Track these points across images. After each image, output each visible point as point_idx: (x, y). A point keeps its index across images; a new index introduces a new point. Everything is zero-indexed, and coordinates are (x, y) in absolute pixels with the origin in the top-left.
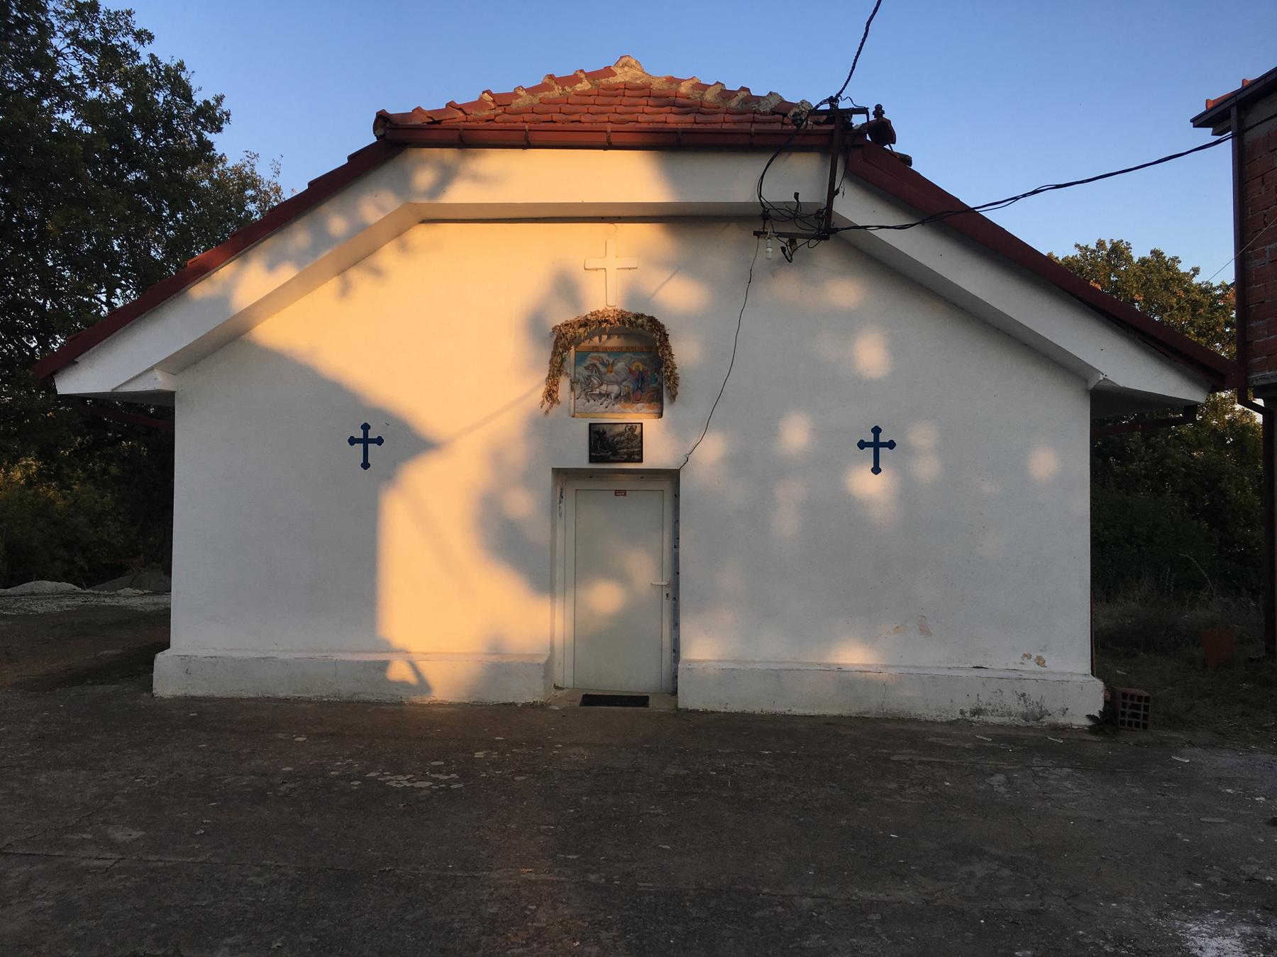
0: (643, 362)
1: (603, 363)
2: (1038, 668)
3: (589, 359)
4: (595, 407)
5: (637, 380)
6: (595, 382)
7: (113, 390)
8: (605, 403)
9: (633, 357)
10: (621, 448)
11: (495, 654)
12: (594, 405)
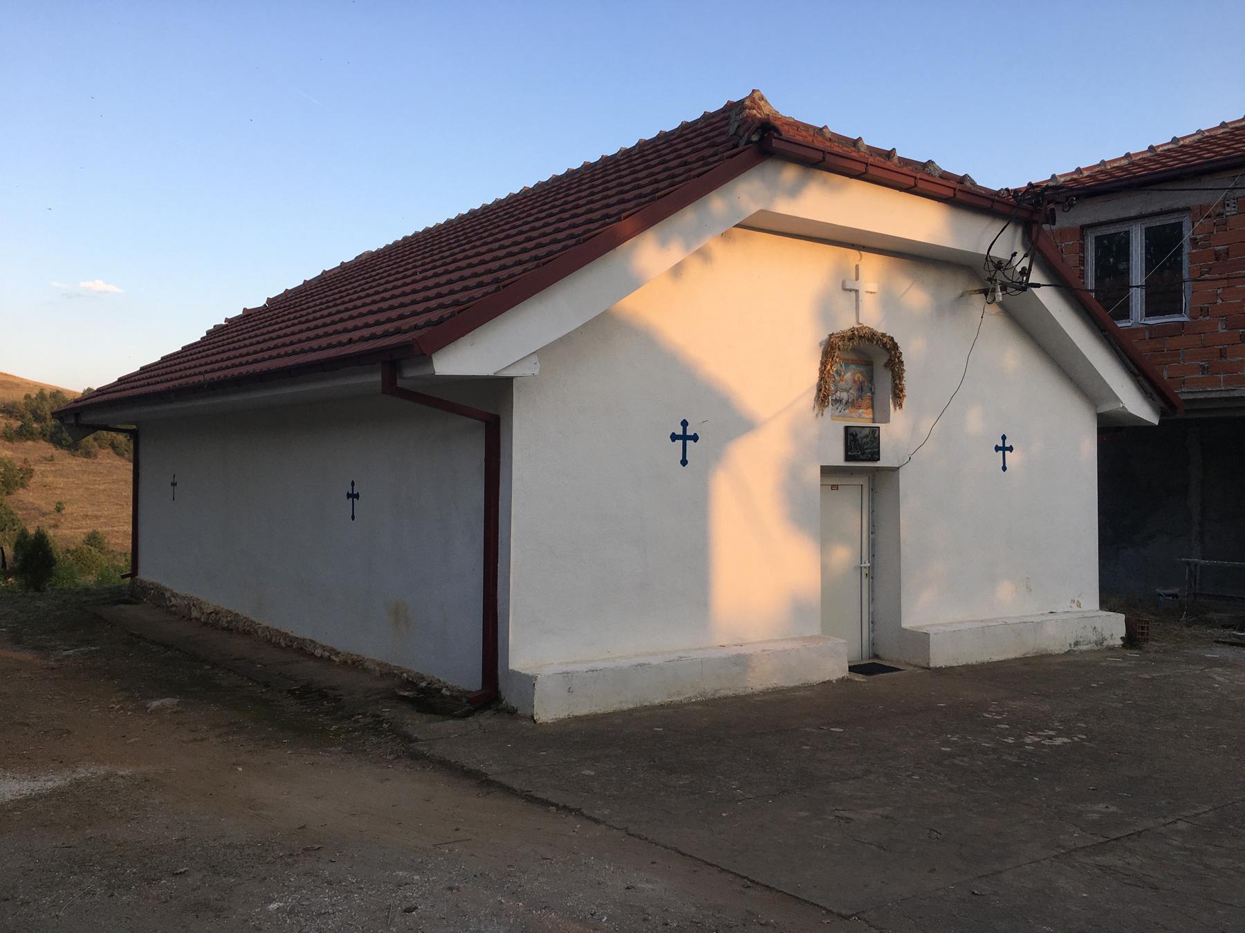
2: (1078, 609)
7: (495, 373)
10: (866, 449)
11: (793, 639)
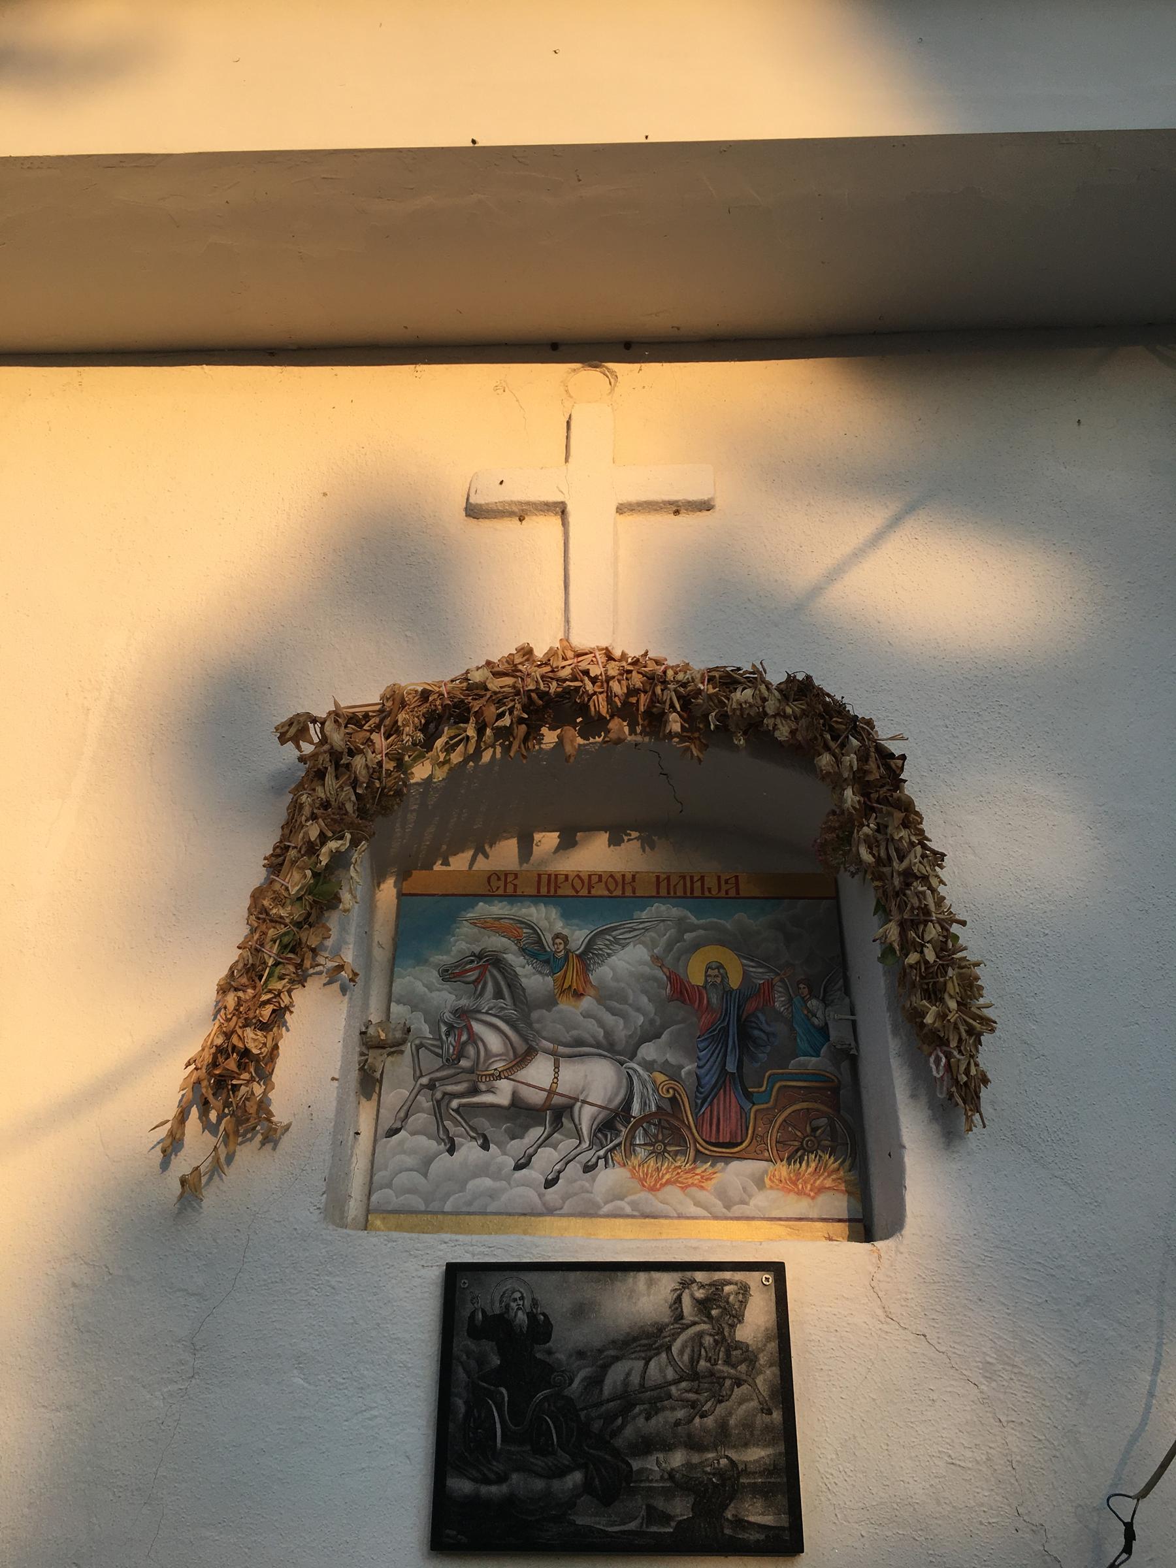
0: (740, 944)
1: (536, 951)
3: (466, 929)
4: (487, 1182)
5: (717, 1037)
6: (494, 1042)
8: (547, 1158)
9: (693, 920)
10: (647, 1446)
12: (482, 1170)
